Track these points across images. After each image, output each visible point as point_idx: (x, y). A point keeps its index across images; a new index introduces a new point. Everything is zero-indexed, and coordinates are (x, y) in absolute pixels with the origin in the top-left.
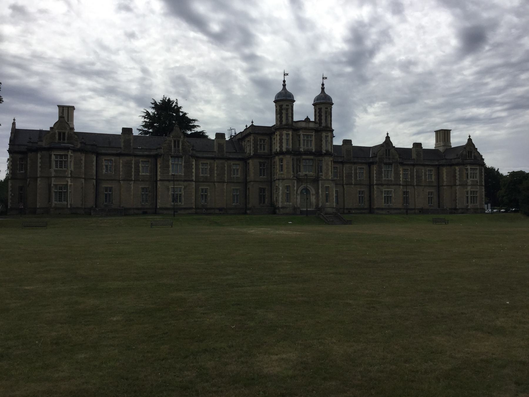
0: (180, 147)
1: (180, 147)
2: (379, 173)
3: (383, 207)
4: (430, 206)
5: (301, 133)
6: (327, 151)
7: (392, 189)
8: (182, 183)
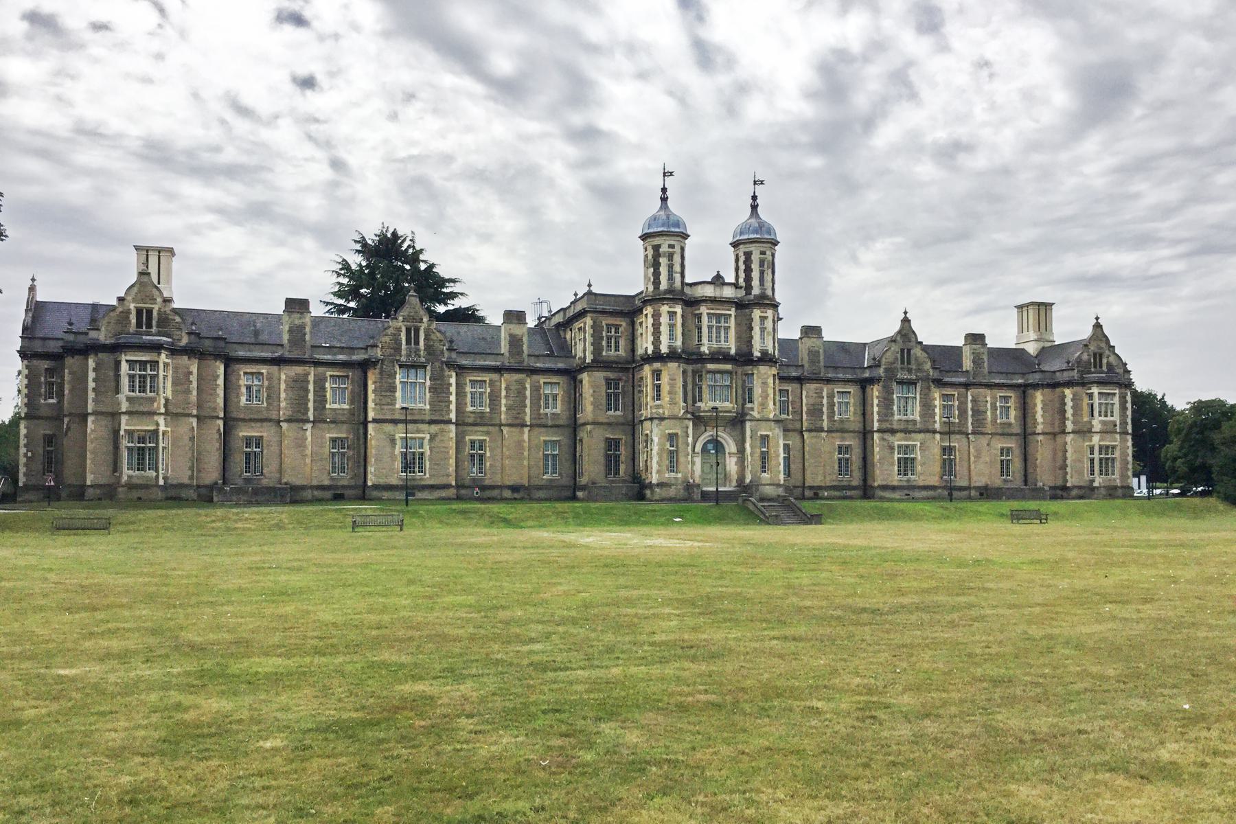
0: (422, 343)
2: (887, 403)
3: (895, 483)
4: (1005, 481)
5: (704, 310)
6: (764, 353)
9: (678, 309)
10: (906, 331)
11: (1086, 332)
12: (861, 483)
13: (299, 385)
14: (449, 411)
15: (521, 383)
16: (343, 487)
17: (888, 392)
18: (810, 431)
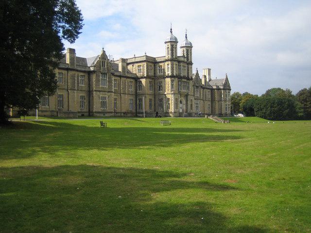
0: (106, 66)
1: (106, 66)
2: (98, 81)
3: (100, 111)
4: (81, 109)
5: (181, 64)
6: (168, 74)
7: (107, 95)
8: (107, 93)
9: (177, 63)
10: (104, 56)
11: (100, 53)
12: (88, 110)
13: (73, 77)
14: (112, 89)
15: (125, 81)
16: (84, 112)
17: (98, 76)
18: (71, 90)
